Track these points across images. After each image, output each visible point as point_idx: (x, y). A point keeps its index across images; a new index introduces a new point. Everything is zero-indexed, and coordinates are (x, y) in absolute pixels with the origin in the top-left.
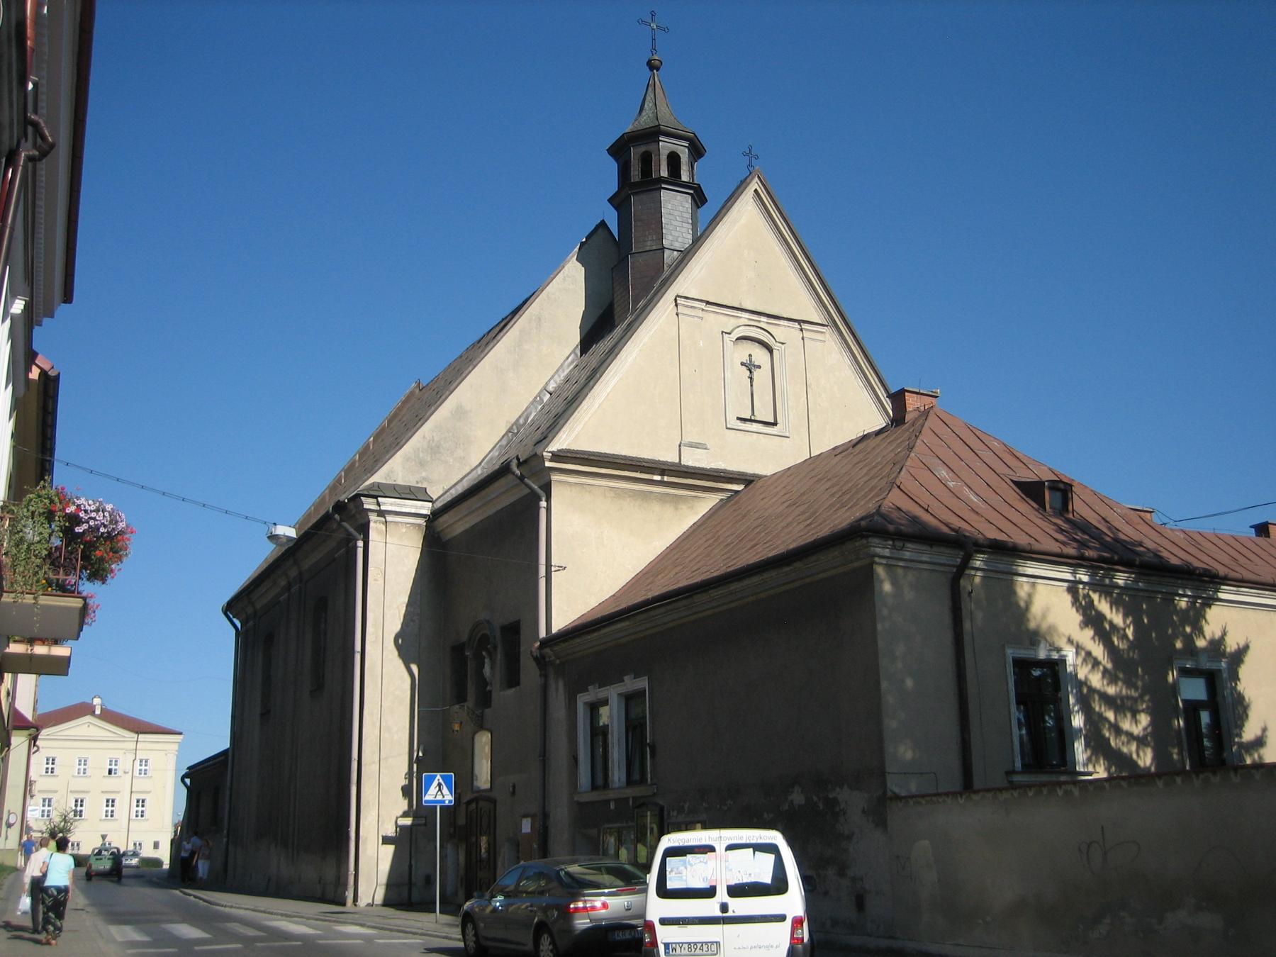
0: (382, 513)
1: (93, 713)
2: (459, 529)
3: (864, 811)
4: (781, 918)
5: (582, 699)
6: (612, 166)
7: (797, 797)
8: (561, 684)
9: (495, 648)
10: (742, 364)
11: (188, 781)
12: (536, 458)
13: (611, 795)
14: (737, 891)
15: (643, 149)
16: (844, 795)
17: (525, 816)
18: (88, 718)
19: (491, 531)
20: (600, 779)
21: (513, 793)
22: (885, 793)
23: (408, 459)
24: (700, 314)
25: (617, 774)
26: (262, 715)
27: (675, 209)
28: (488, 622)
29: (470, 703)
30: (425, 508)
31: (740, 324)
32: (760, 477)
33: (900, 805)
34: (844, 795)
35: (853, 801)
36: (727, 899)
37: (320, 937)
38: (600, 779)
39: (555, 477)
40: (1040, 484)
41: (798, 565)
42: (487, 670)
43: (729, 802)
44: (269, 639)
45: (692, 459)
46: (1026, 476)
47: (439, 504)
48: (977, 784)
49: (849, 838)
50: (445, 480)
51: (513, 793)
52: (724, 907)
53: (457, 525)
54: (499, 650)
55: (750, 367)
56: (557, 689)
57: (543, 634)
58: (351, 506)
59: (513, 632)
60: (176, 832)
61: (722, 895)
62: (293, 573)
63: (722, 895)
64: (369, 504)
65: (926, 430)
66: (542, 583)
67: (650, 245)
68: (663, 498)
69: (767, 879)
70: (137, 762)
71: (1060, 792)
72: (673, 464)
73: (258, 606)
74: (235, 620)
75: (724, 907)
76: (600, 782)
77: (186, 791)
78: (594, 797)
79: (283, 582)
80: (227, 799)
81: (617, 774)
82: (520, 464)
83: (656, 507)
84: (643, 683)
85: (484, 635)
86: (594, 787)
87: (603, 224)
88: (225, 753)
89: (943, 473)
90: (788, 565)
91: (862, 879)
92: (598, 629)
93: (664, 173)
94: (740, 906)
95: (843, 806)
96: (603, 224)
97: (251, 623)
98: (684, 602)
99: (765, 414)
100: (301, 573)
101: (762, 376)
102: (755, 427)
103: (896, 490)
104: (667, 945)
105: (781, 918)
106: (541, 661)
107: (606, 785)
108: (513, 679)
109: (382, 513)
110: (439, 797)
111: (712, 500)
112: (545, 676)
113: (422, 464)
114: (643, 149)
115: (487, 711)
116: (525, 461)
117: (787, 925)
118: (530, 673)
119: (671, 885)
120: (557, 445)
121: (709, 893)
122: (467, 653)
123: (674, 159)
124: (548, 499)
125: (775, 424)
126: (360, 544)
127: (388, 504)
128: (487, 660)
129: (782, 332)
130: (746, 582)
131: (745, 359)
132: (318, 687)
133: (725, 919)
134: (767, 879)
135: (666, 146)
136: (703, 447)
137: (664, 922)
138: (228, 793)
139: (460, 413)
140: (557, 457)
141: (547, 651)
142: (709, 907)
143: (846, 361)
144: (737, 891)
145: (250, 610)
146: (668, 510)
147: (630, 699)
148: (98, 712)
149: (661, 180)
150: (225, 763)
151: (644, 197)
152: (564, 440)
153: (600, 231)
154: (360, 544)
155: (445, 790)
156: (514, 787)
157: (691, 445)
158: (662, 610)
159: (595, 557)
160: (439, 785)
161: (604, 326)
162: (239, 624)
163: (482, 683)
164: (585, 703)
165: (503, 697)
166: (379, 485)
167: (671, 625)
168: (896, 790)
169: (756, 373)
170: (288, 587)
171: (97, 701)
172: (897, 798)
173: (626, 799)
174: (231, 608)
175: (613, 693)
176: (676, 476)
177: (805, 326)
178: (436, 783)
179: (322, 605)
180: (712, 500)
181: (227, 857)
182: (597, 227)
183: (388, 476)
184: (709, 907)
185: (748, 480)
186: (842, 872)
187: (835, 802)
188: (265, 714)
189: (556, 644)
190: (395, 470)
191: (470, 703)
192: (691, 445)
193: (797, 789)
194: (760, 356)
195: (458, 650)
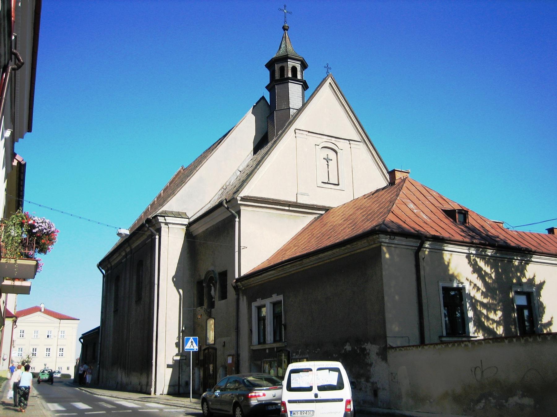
0: (167, 224)
1: (41, 311)
3: (377, 354)
4: (341, 400)
5: (254, 305)
6: (267, 73)
7: (348, 347)
8: (245, 298)
9: (216, 282)
10: (324, 159)
11: (82, 340)
13: (267, 346)
14: (322, 388)
15: (281, 65)
16: (368, 346)
17: (229, 355)
18: (39, 313)
19: (215, 230)
20: (262, 340)
21: (224, 346)
22: (386, 345)
24: (306, 137)
25: (270, 337)
26: (114, 312)
28: (213, 271)
29: (205, 306)
30: (186, 222)
31: (323, 141)
32: (332, 208)
33: (393, 350)
34: (368, 346)
35: (373, 349)
37: (140, 408)
38: (262, 340)
39: (242, 208)
40: (454, 211)
41: (348, 246)
42: (213, 292)
43: (318, 350)
44: (118, 279)
46: (448, 207)
47: (191, 220)
49: (371, 365)
51: (224, 346)
52: (316, 396)
53: (199, 229)
54: (218, 281)
55: (327, 160)
56: (243, 300)
57: (237, 276)
58: (153, 220)
59: (224, 275)
61: (315, 390)
62: (128, 250)
63: (315, 390)
64: (161, 219)
65: (404, 187)
67: (284, 107)
70: (60, 332)
71: (463, 345)
72: (294, 203)
73: (113, 264)
74: (103, 270)
75: (316, 396)
76: (262, 341)
77: (81, 344)
78: (260, 347)
79: (123, 254)
80: (99, 348)
81: (270, 337)
82: (227, 202)
84: (281, 298)
85: (211, 277)
86: (259, 343)
87: (263, 98)
88: (98, 328)
89: (411, 206)
90: (344, 246)
91: (376, 383)
92: (261, 274)
95: (368, 351)
96: (263, 98)
97: (110, 272)
98: (299, 262)
99: (334, 180)
100: (131, 250)
101: (332, 164)
103: (391, 214)
104: (291, 412)
105: (341, 400)
106: (236, 288)
107: (264, 342)
108: (224, 296)
109: (167, 224)
110: (192, 348)
111: (311, 218)
112: (238, 295)
114: (281, 65)
115: (213, 310)
116: (229, 201)
117: (344, 403)
118: (231, 293)
119: (293, 385)
122: (204, 285)
123: (294, 69)
124: (239, 218)
125: (338, 185)
126: (157, 237)
127: (169, 220)
128: (213, 288)
129: (341, 144)
130: (326, 254)
132: (139, 299)
133: (317, 401)
137: (290, 402)
138: (99, 345)
140: (243, 199)
141: (239, 283)
142: (309, 395)
144: (322, 388)
145: (109, 266)
147: (275, 305)
148: (43, 310)
149: (288, 78)
152: (246, 192)
153: (262, 101)
154: (157, 237)
155: (194, 344)
156: (224, 343)
158: (289, 266)
159: (260, 242)
160: (192, 342)
161: (263, 142)
162: (104, 272)
163: (210, 298)
164: (256, 307)
165: (219, 304)
167: (293, 272)
168: (391, 344)
169: (330, 162)
170: (126, 255)
172: (392, 348)
173: (274, 348)
175: (268, 302)
177: (351, 142)
178: (190, 341)
179: (140, 264)
180: (311, 218)
181: (99, 373)
182: (261, 99)
184: (309, 395)
185: (327, 209)
186: (367, 380)
187: (365, 349)
188: (116, 311)
189: (243, 281)
190: (171, 205)
191: (205, 306)
193: (348, 344)
194: (332, 155)
195: (200, 283)
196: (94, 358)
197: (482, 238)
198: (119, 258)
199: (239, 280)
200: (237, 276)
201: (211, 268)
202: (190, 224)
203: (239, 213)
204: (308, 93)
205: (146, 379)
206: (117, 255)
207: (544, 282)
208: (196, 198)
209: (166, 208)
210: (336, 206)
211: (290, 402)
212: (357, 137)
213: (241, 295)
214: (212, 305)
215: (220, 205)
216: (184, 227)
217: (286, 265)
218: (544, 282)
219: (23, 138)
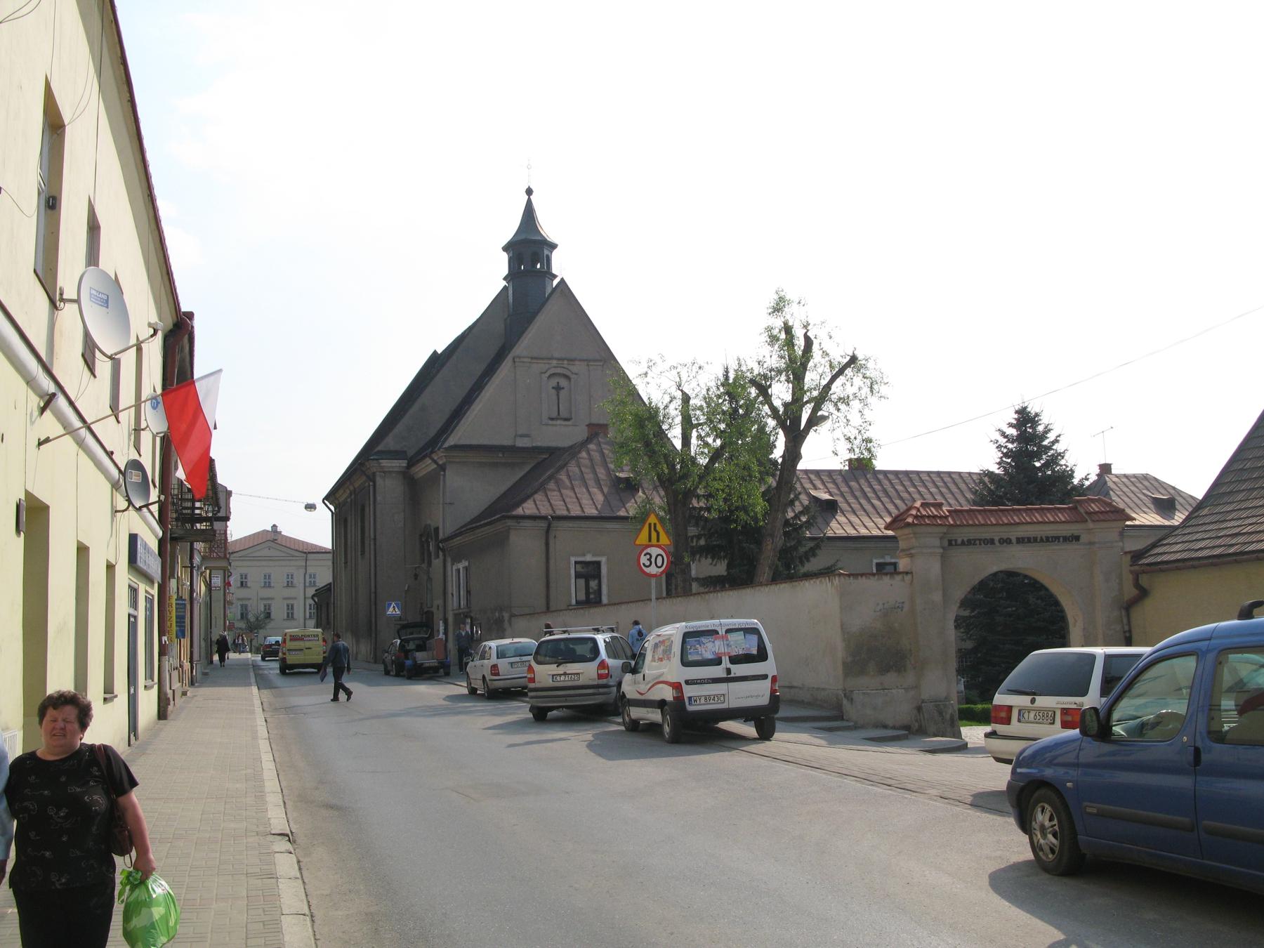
2: (421, 474)
4: (765, 677)
5: (455, 568)
6: (504, 257)
14: (735, 660)
36: (729, 666)
44: (346, 521)
45: (521, 443)
48: (553, 606)
52: (729, 671)
55: (558, 388)
59: (437, 529)
61: (725, 660)
63: (725, 660)
69: (755, 652)
75: (729, 671)
94: (739, 670)
99: (564, 414)
102: (559, 422)
104: (690, 698)
105: (765, 677)
108: (438, 557)
117: (768, 683)
119: (691, 658)
121: (717, 662)
131: (555, 384)
132: (363, 553)
133: (729, 679)
134: (755, 652)
137: (687, 682)
142: (718, 671)
144: (735, 660)
150: (329, 589)
157: (521, 436)
165: (437, 563)
174: (505, 249)
179: (363, 509)
184: (718, 671)
188: (346, 563)
190: (390, 443)
192: (521, 436)
194: (563, 383)
195: (421, 536)
196: (328, 623)
197: (824, 394)
198: (345, 496)
201: (429, 522)
206: (341, 492)
207: (1025, 419)
211: (687, 682)
213: (449, 560)
214: (430, 564)
217: (482, 526)
218: (1025, 419)
219: (134, 783)
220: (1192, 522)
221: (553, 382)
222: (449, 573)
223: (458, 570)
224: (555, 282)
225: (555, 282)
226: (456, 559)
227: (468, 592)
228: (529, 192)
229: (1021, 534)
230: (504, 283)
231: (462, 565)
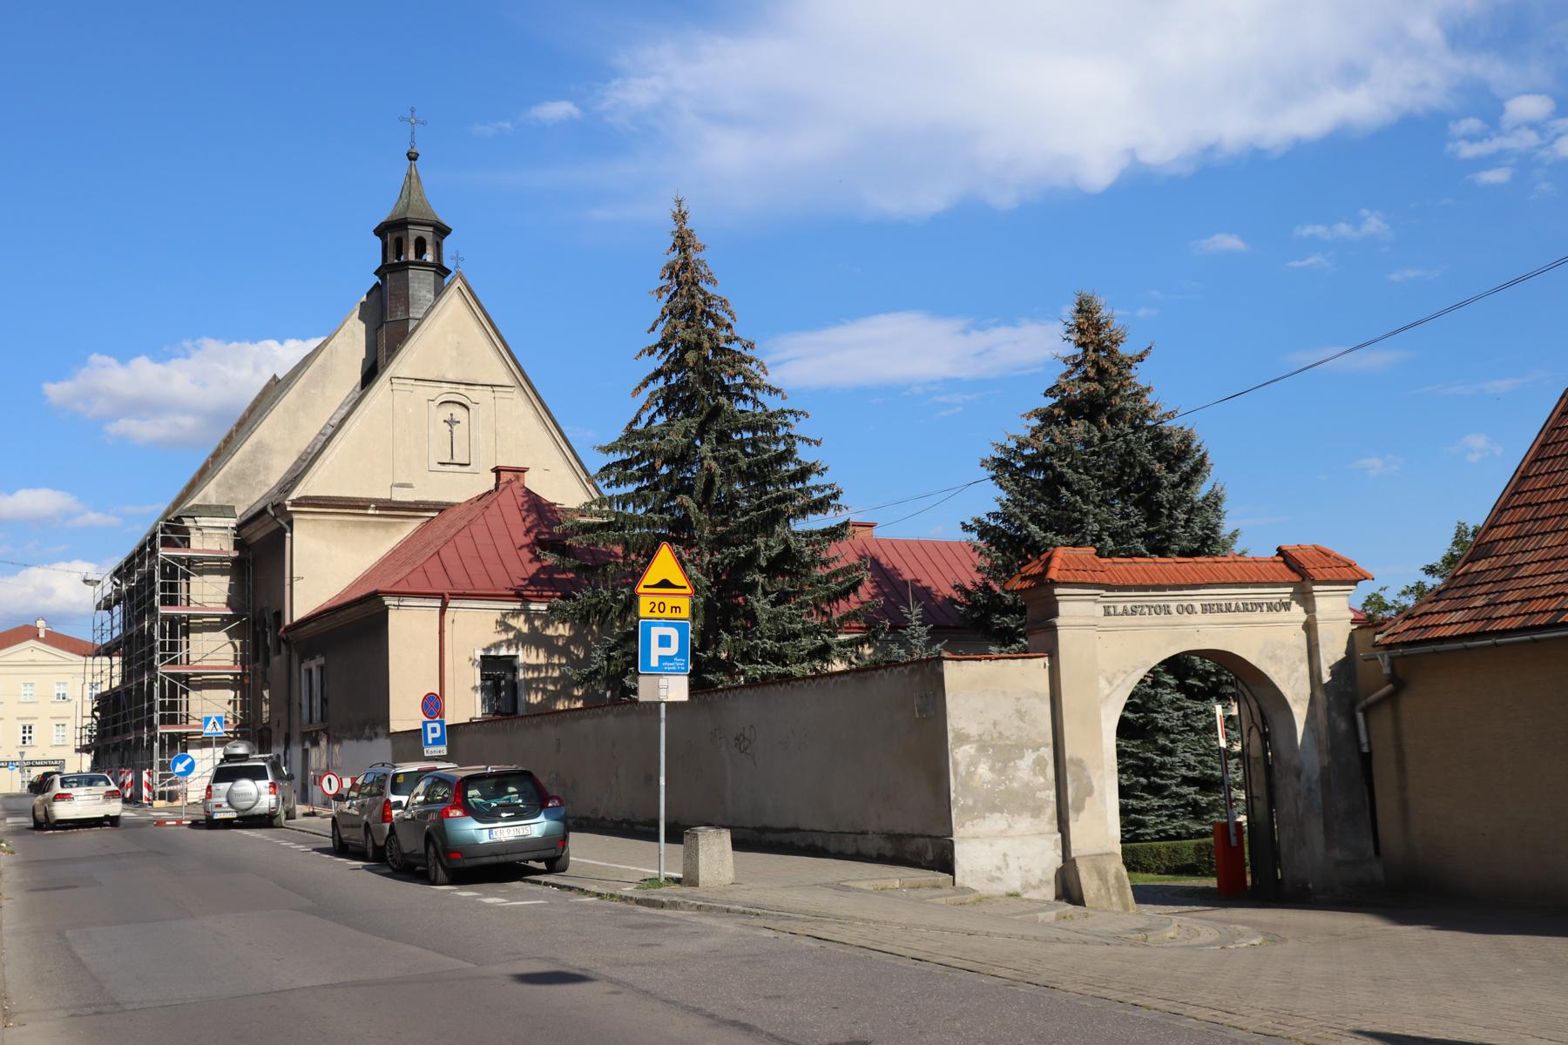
0: (199, 529)
1: (37, 637)
5: (304, 666)
6: (378, 242)
12: (279, 506)
15: (396, 235)
18: (32, 643)
19: (261, 551)
23: (218, 485)
25: (317, 715)
27: (420, 284)
30: (232, 522)
39: (295, 516)
50: (247, 500)
53: (257, 534)
55: (451, 422)
57: (288, 622)
59: (279, 615)
60: (997, 325)
64: (188, 523)
66: (287, 589)
67: (400, 316)
68: (376, 525)
83: (372, 531)
84: (320, 660)
93: (412, 256)
102: (451, 467)
108: (279, 652)
109: (199, 529)
111: (410, 527)
113: (231, 488)
114: (396, 235)
118: (283, 647)
120: (294, 495)
127: (203, 521)
129: (475, 394)
131: (448, 417)
135: (414, 233)
136: (409, 486)
139: (260, 448)
140: (294, 503)
143: (531, 411)
146: (381, 533)
147: (322, 668)
148: (42, 635)
149: (408, 263)
151: (397, 275)
152: (314, 485)
163: (267, 649)
165: (276, 660)
166: (198, 506)
171: (40, 624)
174: (381, 231)
176: (391, 509)
180: (410, 527)
183: (205, 498)
185: (441, 508)
190: (210, 493)
194: (459, 413)
199: (287, 629)
200: (288, 622)
202: (239, 527)
203: (290, 523)
204: (447, 280)
205: (1076, 849)
208: (244, 486)
209: (196, 500)
210: (462, 500)
212: (507, 381)
214: (267, 662)
215: (263, 511)
216: (231, 533)
220: (1549, 452)
221: (446, 412)
222: (295, 674)
223: (310, 672)
224: (1130, 716)
225: (1130, 716)
226: (308, 654)
227: (324, 701)
228: (412, 157)
229: (1208, 600)
230: (376, 279)
231: (314, 664)
